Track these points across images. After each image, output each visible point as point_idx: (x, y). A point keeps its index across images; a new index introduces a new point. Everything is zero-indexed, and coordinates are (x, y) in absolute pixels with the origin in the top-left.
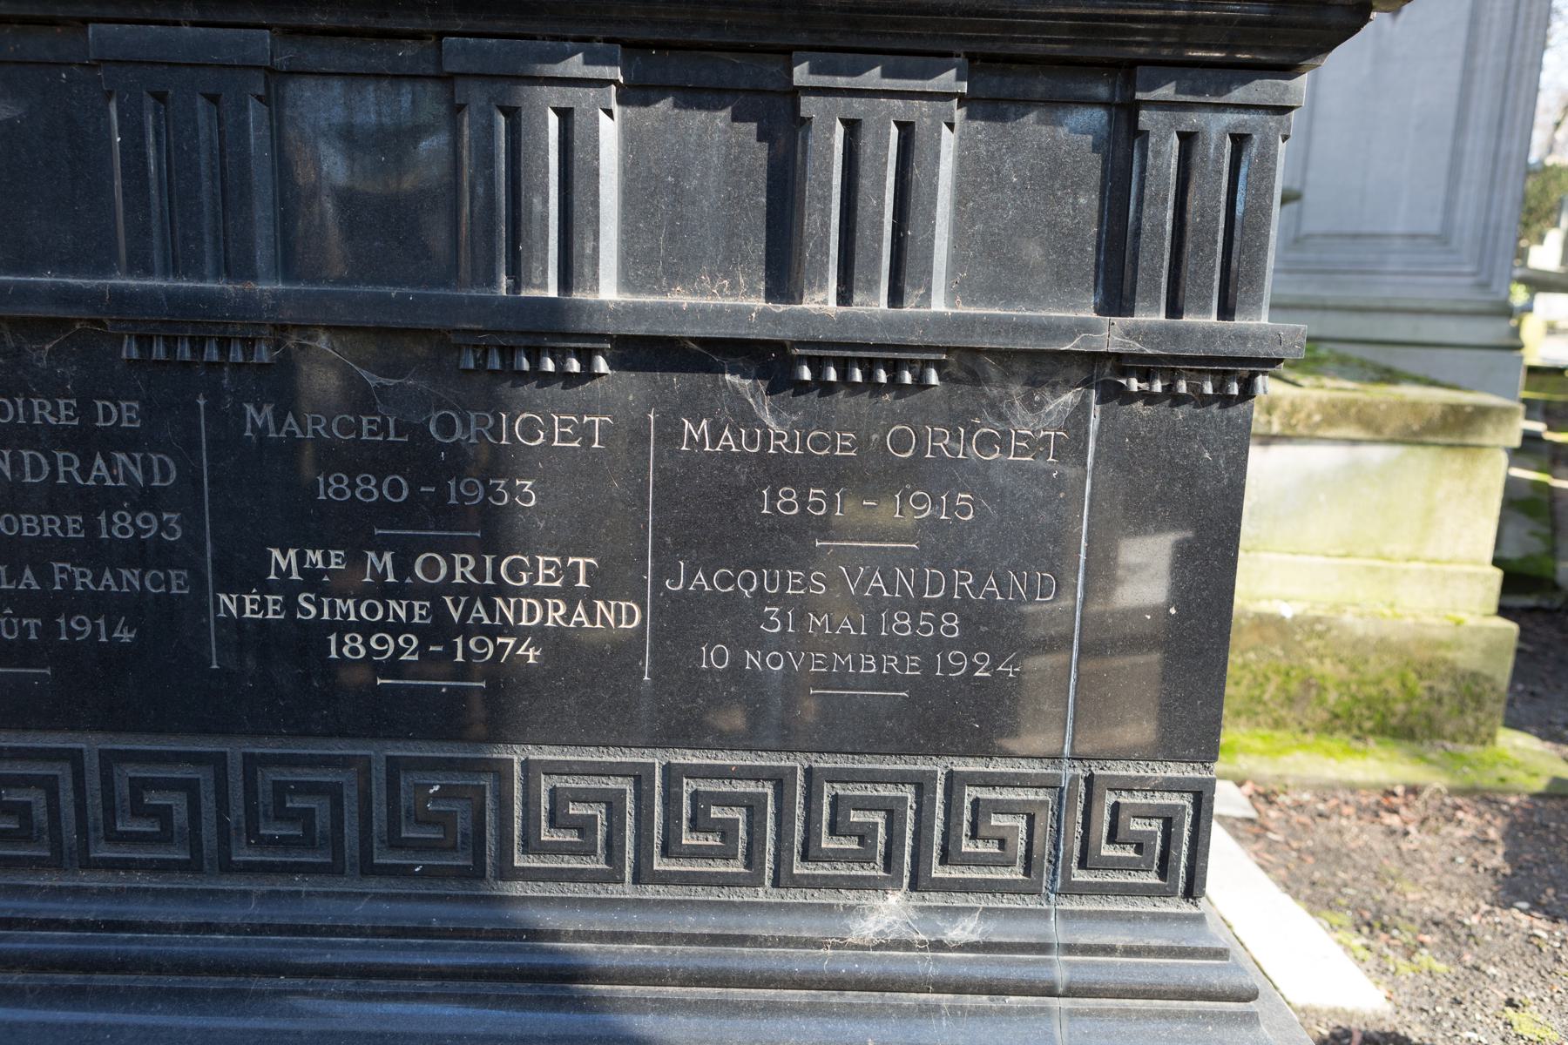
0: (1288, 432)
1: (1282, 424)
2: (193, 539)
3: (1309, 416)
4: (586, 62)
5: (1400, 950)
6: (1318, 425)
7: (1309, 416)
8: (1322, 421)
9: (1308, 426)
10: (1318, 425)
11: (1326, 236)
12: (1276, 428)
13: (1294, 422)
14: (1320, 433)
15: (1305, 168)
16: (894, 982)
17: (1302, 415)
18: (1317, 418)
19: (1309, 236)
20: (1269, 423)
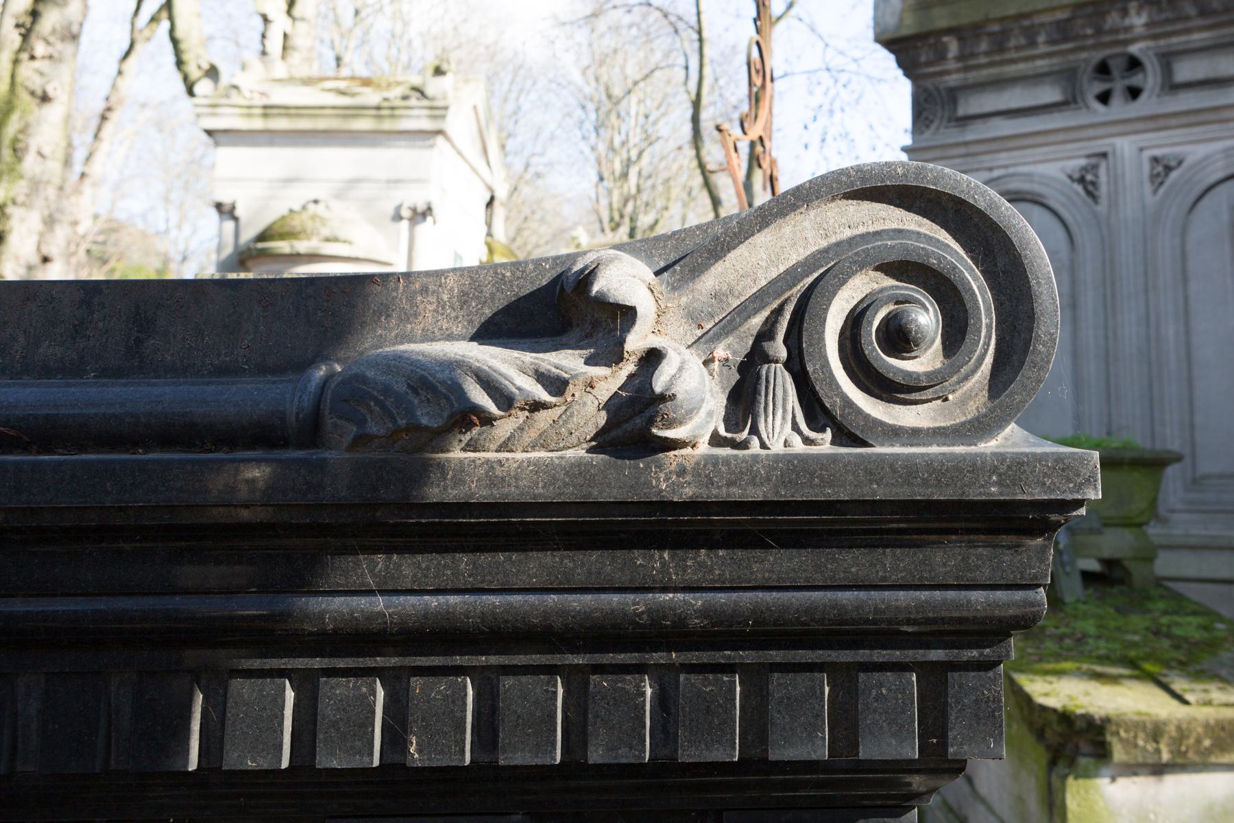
0: (1179, 761)
1: (1171, 752)
2: (745, 670)
3: (1199, 741)
4: (834, 442)
5: (23, 123)
6: (1209, 751)
7: (1199, 741)
8: (1212, 745)
9: (1198, 752)
10: (1209, 751)
11: (1222, 476)
12: (1166, 756)
13: (1183, 748)
14: (1213, 759)
15: (1192, 413)
16: (947, 436)
17: (1191, 741)
18: (1207, 743)
19: (1207, 477)
20: (1158, 751)
